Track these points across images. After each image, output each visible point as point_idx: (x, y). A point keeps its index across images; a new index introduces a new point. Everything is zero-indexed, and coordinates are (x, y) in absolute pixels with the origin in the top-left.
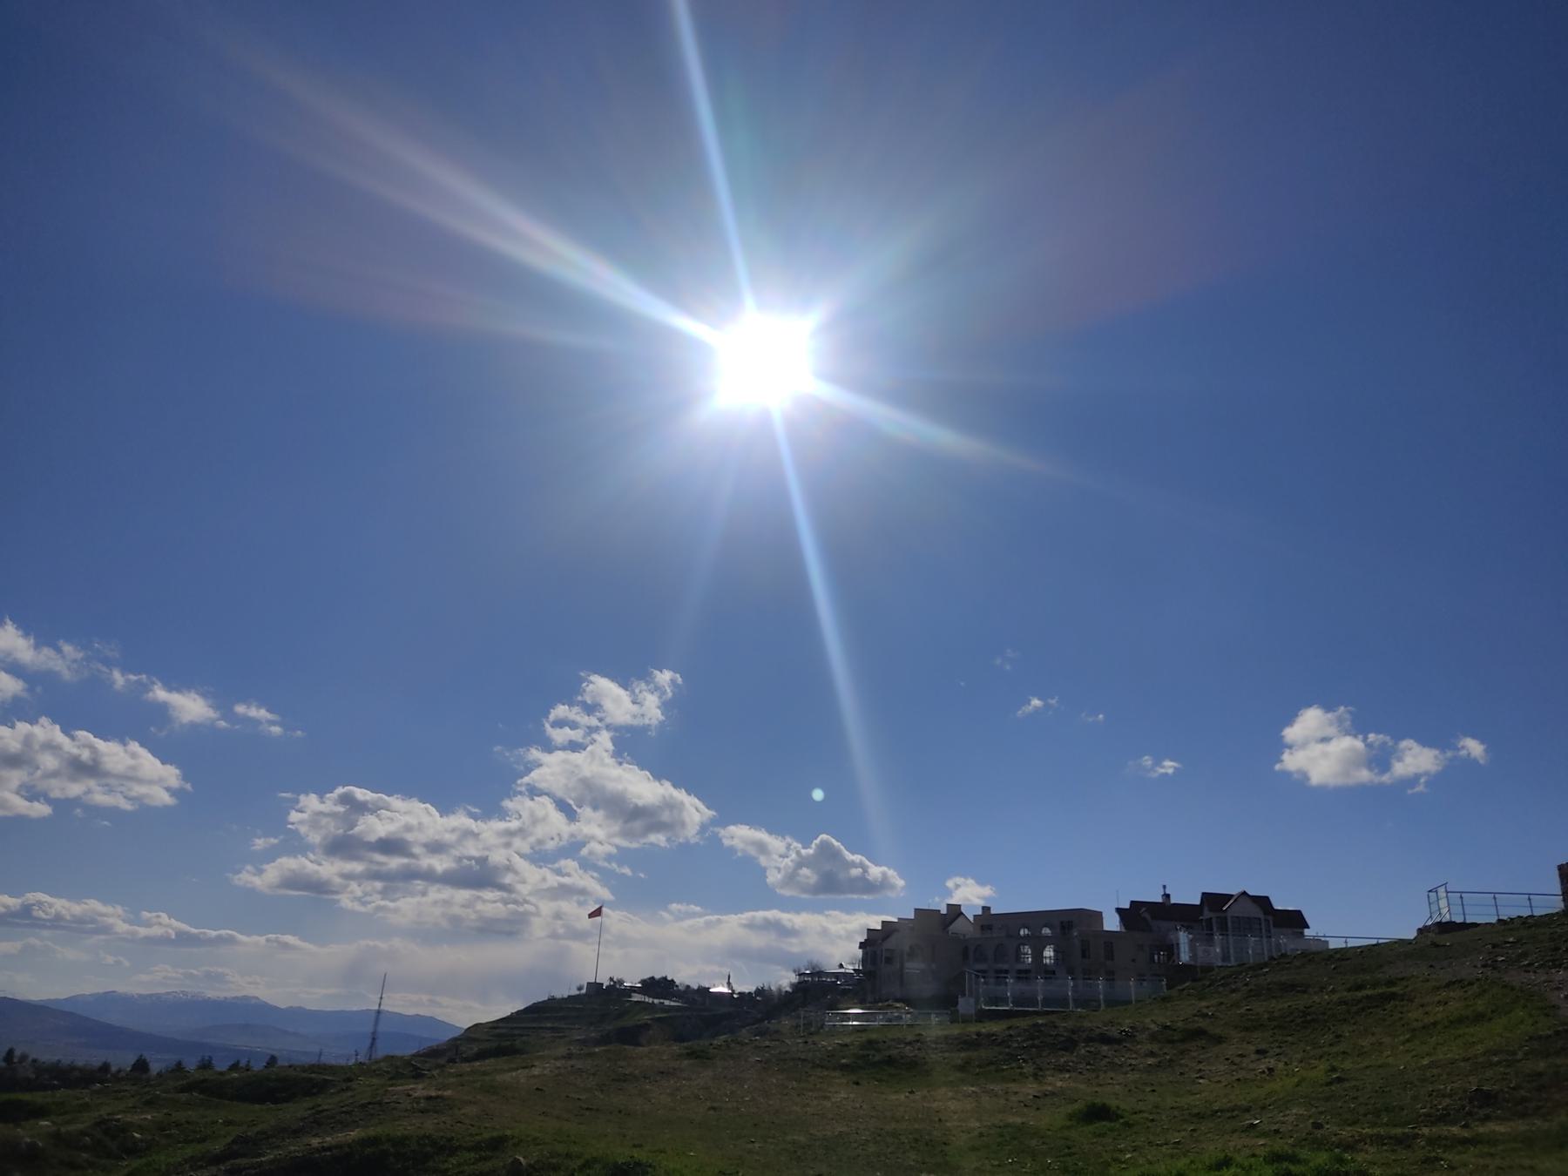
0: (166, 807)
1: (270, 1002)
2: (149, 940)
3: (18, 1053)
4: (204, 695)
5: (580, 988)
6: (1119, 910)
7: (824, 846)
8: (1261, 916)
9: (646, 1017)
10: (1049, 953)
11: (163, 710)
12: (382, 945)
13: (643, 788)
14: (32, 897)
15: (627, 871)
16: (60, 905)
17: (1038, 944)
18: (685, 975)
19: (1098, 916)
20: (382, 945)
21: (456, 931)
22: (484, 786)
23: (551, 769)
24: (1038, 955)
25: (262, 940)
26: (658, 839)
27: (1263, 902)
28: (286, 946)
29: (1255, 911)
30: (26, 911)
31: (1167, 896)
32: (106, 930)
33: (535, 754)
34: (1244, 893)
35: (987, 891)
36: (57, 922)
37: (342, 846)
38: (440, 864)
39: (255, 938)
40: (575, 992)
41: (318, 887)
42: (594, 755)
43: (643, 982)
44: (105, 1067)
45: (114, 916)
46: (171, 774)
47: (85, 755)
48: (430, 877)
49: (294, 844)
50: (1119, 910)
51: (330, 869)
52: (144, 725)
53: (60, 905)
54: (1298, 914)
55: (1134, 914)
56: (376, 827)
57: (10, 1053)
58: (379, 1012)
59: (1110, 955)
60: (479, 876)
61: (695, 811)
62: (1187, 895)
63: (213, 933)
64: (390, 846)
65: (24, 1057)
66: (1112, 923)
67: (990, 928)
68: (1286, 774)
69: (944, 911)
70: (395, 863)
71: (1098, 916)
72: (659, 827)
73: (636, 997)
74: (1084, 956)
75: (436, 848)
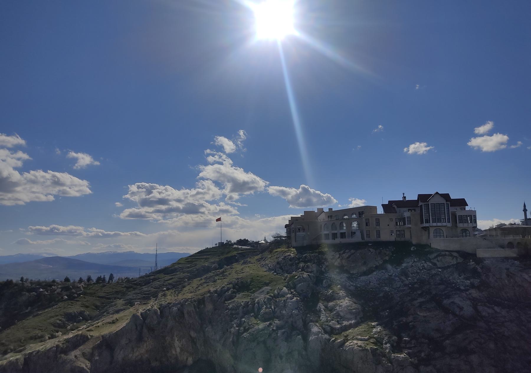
0: (90, 194)
1: (138, 252)
2: (92, 237)
3: (25, 278)
4: (90, 155)
5: (216, 245)
6: (383, 205)
7: (304, 189)
8: (445, 202)
9: (235, 253)
10: (355, 224)
11: (75, 160)
12: (166, 233)
13: (241, 175)
14: (52, 226)
15: (240, 204)
16: (62, 228)
17: (349, 222)
18: (251, 238)
19: (375, 208)
20: (166, 233)
21: (186, 228)
22: (188, 179)
23: (208, 171)
24: (349, 225)
25: (128, 233)
26: (252, 192)
27: (446, 196)
28: (136, 234)
29: (442, 201)
30: (52, 230)
31: (405, 197)
32: (80, 234)
33: (201, 167)
34: (437, 193)
35: (363, 201)
36: (63, 233)
37: (145, 203)
38: (181, 206)
39: (126, 233)
40: (214, 246)
41: (139, 216)
42: (221, 166)
43: (238, 241)
44: (54, 281)
45: (80, 229)
46: (85, 183)
47: (33, 178)
48: (177, 210)
49: (129, 204)
50: (383, 205)
51: (143, 210)
52: (67, 166)
53: (62, 228)
54: (463, 200)
55: (389, 207)
56: (156, 195)
57: (22, 279)
58: (156, 255)
59: (378, 223)
60: (192, 209)
61: (261, 183)
62: (412, 197)
63: (112, 233)
64: (163, 201)
65: (27, 280)
66: (380, 211)
67: (331, 216)
68: (470, 146)
69: (316, 211)
70: (163, 207)
71: (375, 208)
72: (251, 188)
73: (235, 246)
74: (367, 225)
75: (179, 201)
